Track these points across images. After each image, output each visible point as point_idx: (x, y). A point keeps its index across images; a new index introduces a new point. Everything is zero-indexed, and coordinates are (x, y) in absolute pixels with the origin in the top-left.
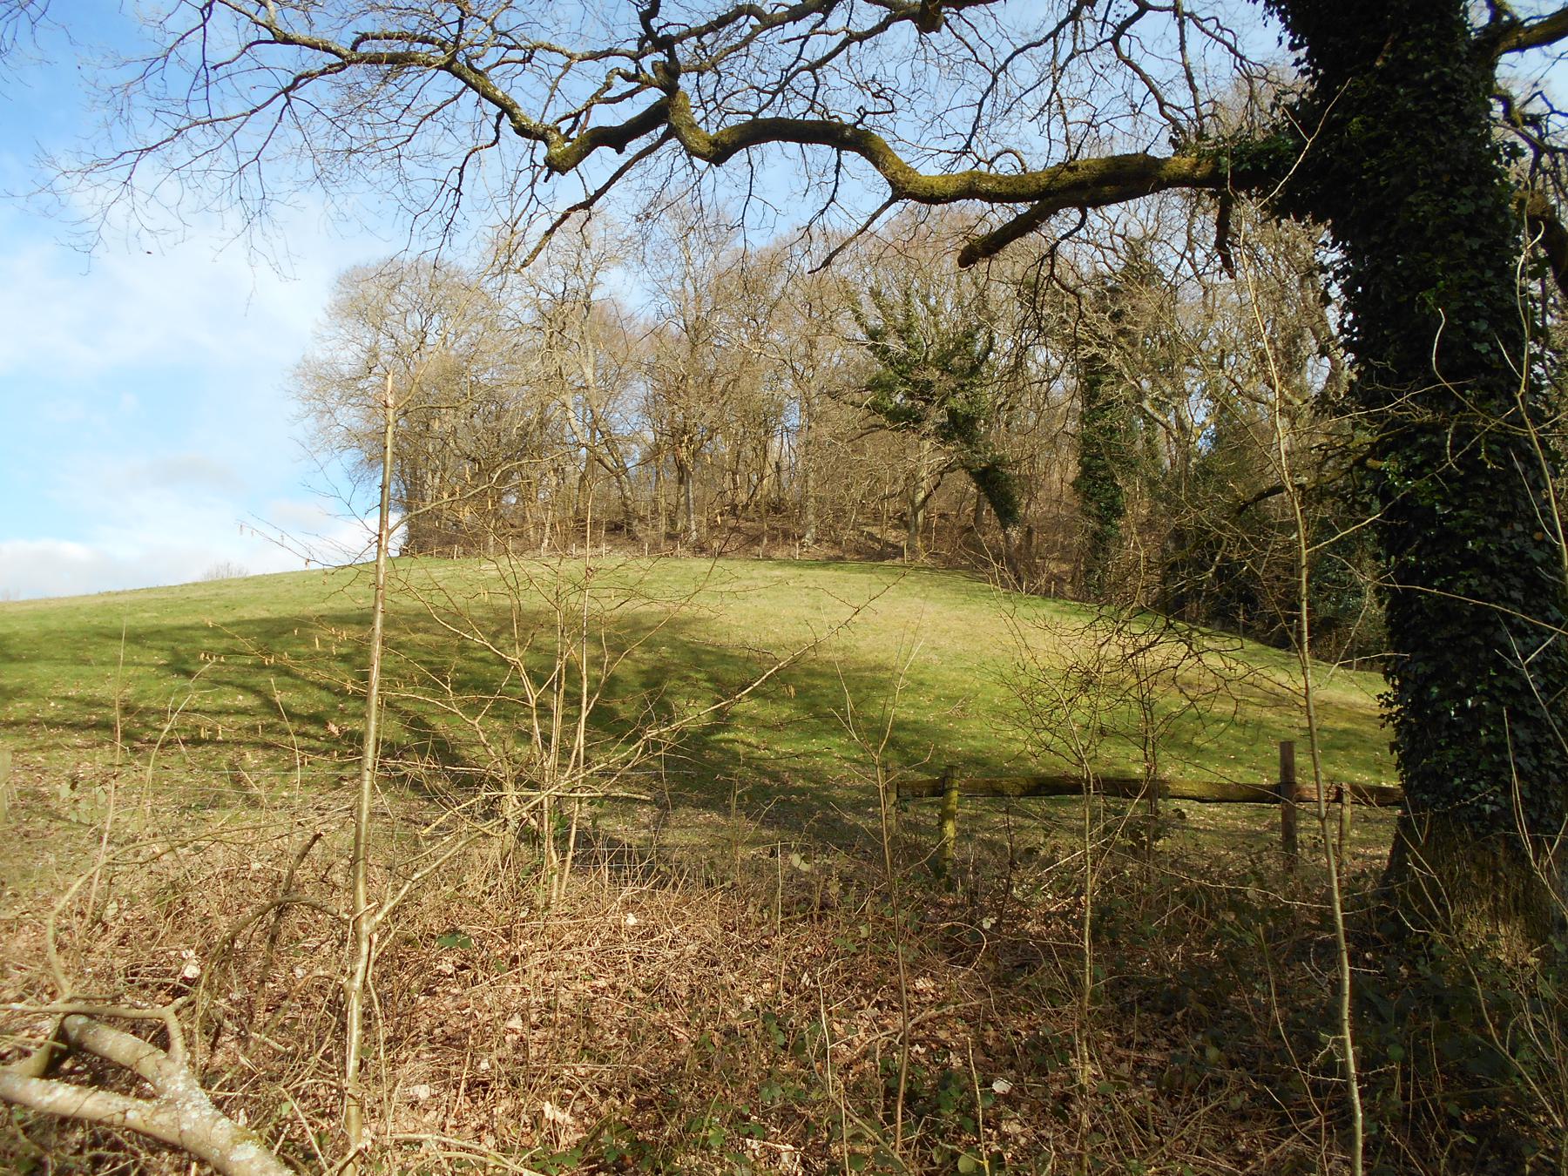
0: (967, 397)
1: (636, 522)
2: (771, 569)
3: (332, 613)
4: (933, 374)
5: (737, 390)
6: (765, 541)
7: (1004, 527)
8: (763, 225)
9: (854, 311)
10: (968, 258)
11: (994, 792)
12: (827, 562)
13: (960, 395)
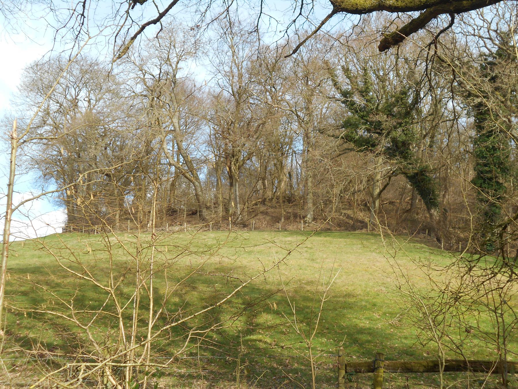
0: (403, 130)
1: (204, 210)
2: (286, 237)
3: (18, 267)
4: (382, 117)
5: (264, 130)
6: (283, 220)
7: (429, 209)
8: (270, 30)
9: (333, 80)
10: (384, 46)
11: (407, 369)
12: (318, 233)
13: (400, 130)
